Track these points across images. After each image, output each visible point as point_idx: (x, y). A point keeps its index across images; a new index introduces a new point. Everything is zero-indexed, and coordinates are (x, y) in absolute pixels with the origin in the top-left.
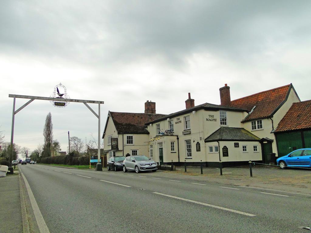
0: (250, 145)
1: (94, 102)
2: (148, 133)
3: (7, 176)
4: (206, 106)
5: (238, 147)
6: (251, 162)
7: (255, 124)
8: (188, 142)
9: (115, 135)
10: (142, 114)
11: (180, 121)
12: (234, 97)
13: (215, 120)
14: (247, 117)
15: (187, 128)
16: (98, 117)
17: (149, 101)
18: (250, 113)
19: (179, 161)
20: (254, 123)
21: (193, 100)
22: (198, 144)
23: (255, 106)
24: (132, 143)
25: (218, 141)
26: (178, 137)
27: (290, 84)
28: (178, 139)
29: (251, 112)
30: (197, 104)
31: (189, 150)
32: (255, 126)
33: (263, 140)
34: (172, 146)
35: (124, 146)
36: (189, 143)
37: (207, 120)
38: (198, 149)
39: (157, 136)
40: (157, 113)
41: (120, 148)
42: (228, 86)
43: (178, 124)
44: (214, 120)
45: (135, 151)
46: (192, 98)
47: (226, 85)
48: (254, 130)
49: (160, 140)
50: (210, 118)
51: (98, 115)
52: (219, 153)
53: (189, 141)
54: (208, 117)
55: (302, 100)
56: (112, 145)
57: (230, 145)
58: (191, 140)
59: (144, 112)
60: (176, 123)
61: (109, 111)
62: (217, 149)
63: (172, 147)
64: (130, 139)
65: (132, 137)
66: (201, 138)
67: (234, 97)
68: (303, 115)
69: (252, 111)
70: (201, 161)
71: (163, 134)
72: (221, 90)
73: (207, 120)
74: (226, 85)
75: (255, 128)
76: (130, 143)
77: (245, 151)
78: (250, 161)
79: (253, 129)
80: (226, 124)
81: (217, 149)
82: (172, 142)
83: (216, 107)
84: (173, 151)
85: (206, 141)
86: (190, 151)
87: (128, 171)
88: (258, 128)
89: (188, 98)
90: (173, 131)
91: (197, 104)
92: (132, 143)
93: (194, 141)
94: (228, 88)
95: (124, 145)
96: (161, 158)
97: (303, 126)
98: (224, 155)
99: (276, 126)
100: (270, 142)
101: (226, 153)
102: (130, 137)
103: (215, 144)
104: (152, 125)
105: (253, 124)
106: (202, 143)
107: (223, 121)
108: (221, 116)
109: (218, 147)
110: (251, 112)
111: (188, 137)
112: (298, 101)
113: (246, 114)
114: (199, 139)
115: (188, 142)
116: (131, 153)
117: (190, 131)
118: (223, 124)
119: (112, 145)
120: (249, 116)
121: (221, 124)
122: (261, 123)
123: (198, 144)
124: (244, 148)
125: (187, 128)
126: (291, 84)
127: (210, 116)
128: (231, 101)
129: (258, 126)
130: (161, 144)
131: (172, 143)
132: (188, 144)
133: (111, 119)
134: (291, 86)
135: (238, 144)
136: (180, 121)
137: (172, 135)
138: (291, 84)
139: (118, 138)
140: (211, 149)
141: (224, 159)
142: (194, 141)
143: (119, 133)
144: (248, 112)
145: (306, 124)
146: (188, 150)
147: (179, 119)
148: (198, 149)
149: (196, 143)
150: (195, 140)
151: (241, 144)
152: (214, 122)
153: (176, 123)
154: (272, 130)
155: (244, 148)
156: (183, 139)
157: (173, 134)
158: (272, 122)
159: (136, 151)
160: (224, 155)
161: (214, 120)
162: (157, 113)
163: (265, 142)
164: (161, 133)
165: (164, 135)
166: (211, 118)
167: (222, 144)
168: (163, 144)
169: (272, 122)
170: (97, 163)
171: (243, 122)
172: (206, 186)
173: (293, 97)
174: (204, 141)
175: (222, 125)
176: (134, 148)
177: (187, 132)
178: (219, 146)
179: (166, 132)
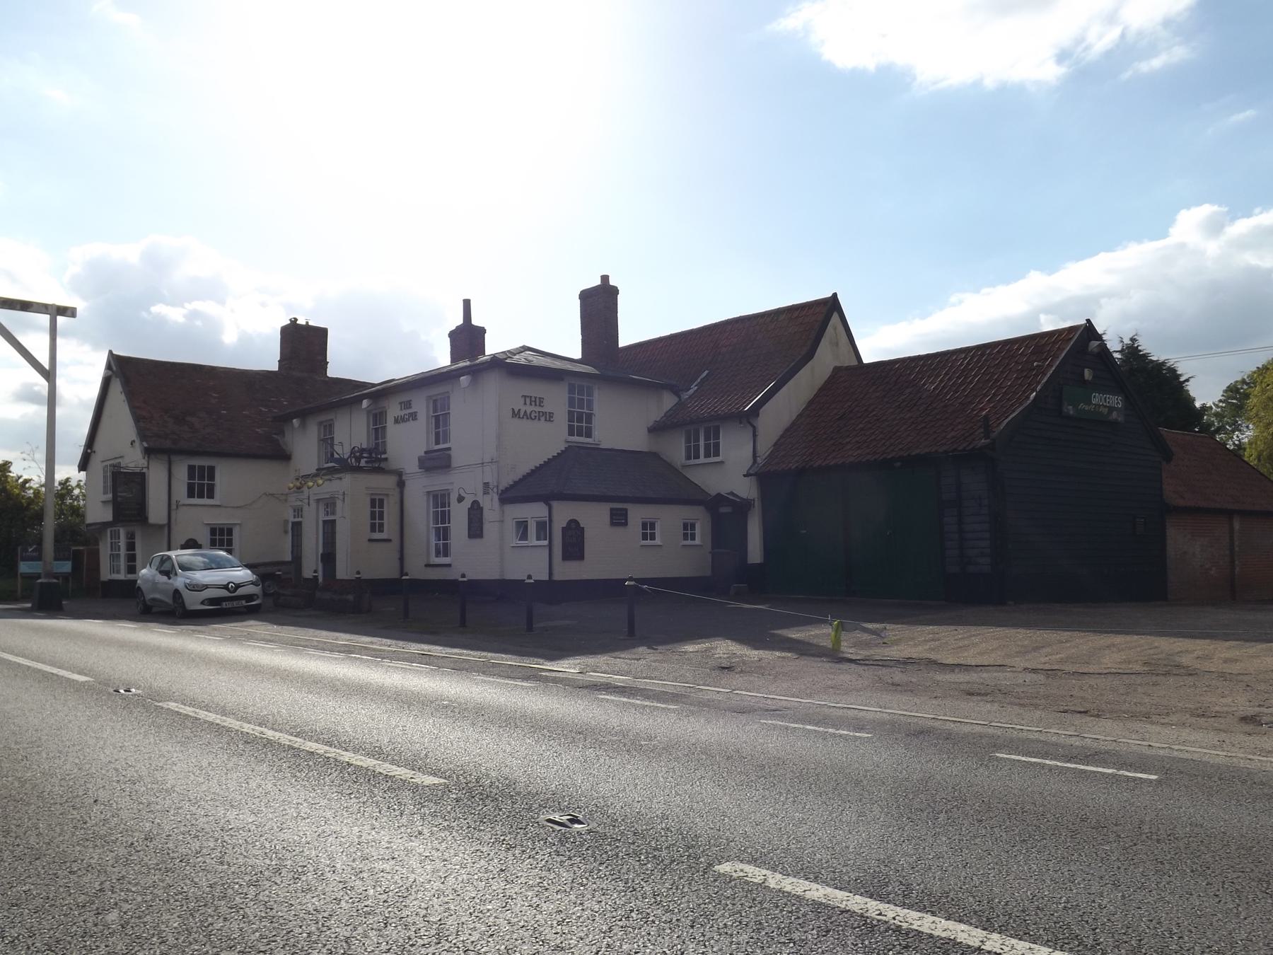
0: (669, 519)
1: (25, 306)
2: (283, 456)
3: (593, 436)
4: (520, 359)
5: (626, 524)
6: (632, 583)
7: (697, 440)
8: (440, 500)
9: (134, 458)
10: (266, 375)
11: (411, 414)
12: (630, 333)
13: (549, 417)
14: (670, 414)
15: (437, 443)
16: (49, 374)
17: (301, 321)
18: (685, 396)
19: (551, 574)
20: (692, 439)
21: (481, 332)
22: (476, 513)
23: (706, 372)
24: (211, 496)
25: (547, 499)
26: (404, 478)
27: (830, 295)
28: (401, 484)
29: (691, 392)
30: (493, 346)
31: (443, 534)
32: (697, 448)
33: (720, 499)
34: (381, 517)
35: (174, 507)
36: (443, 505)
37: (516, 414)
38: (476, 529)
39: (320, 472)
40: (332, 372)
41: (156, 511)
42: (612, 283)
43: (402, 425)
44: (543, 419)
45: (222, 531)
46: (476, 321)
47: (605, 279)
48: (693, 462)
49: (327, 487)
50: (529, 409)
51: (47, 367)
52: (550, 546)
53: (443, 496)
54: (519, 405)
55: (866, 359)
56: (119, 499)
57: (594, 517)
58: (449, 494)
59: (276, 369)
60: (397, 421)
61: (111, 352)
62: (544, 529)
63: (373, 516)
64: (201, 478)
65: (212, 470)
66: (486, 485)
67: (630, 333)
68: (859, 415)
69: (694, 388)
70: (463, 576)
71: (341, 461)
72: (586, 296)
73: (516, 414)
74: (605, 279)
75: (697, 457)
76: (201, 496)
77: (649, 542)
78: (631, 579)
79: (688, 458)
80: (589, 435)
81: (544, 529)
82: (377, 497)
83: (558, 365)
84: (377, 536)
85: (510, 496)
86: (446, 538)
87: (154, 610)
88: (707, 455)
89: (460, 321)
90: (385, 452)
91: (493, 346)
92: (211, 496)
93: (460, 499)
94: (614, 292)
95: (173, 502)
96: (329, 558)
97: (850, 453)
98: (567, 556)
99: (765, 447)
100: (741, 508)
101: (574, 544)
102: (202, 468)
103: (534, 512)
104: (303, 425)
105: (688, 441)
106: (490, 505)
107: (580, 422)
108: (571, 402)
109: (546, 522)
110: (691, 392)
111: (438, 482)
112: (855, 363)
113: (669, 401)
114: (480, 488)
115: (440, 500)
116: (203, 536)
117: (449, 456)
118: (580, 434)
119: (119, 499)
120: (680, 405)
121: (571, 433)
122: (717, 436)
123: (476, 513)
124: (648, 529)
125: (437, 443)
126: (835, 295)
127: (528, 401)
128: (620, 346)
129: (707, 447)
130: (329, 504)
131: (377, 503)
132: (447, 509)
133: (117, 388)
134: (831, 306)
135: (624, 513)
136: (414, 416)
137: (380, 470)
138: (835, 295)
139: (144, 470)
140: (522, 527)
141: (568, 571)
142: (460, 499)
143: (148, 452)
144: (676, 391)
145: (859, 448)
146: (438, 530)
147: (407, 405)
148: (476, 529)
149: (467, 504)
150: (463, 494)
151: (637, 514)
152: (542, 425)
153: (397, 421)
154: (751, 463)
155: (648, 529)
156: (418, 489)
157: (383, 465)
158: (755, 436)
159: (230, 532)
160: (567, 556)
161: (543, 419)
162: (332, 372)
163: (725, 510)
164: (336, 461)
165: (346, 466)
166: (533, 408)
167: (564, 513)
168: (339, 504)
169: (755, 436)
170: (39, 576)
171: (657, 429)
172: (1159, 782)
173: (837, 344)
174: (496, 498)
175: (576, 438)
176: (221, 519)
177: (437, 461)
178: (551, 520)
179: (357, 453)
